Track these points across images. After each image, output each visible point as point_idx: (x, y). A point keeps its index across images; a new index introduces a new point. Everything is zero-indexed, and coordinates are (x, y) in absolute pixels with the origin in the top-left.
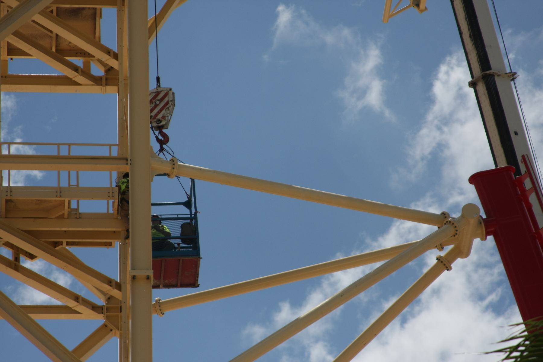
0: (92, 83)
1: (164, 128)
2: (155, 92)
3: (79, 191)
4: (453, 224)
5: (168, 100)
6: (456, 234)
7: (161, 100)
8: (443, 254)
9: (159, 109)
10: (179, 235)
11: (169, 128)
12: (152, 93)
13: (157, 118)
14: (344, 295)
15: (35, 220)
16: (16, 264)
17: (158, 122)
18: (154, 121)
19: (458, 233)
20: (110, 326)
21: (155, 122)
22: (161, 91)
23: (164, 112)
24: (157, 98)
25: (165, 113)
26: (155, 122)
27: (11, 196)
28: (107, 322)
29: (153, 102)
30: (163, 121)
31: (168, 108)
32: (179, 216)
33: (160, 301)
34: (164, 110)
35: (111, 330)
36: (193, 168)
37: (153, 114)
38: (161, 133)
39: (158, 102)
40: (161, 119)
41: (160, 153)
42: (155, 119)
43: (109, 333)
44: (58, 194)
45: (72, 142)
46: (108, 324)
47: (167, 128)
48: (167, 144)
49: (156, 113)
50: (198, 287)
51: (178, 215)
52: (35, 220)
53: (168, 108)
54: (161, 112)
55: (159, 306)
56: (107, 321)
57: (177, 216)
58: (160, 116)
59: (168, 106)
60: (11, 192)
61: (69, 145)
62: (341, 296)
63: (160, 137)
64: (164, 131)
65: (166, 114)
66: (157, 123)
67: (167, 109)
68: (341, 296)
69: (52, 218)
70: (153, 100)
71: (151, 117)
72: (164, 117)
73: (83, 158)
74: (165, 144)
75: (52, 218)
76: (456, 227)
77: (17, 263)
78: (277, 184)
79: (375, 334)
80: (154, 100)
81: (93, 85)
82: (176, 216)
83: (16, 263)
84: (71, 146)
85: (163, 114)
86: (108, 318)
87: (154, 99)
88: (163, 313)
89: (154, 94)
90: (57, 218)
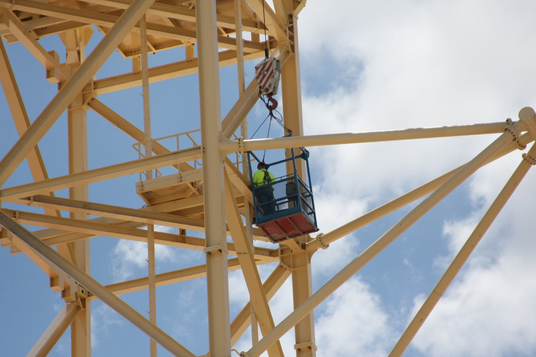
0: (260, 50)
2: (263, 64)
5: (273, 69)
6: (515, 138)
7: (267, 70)
8: (526, 151)
9: (266, 79)
11: (277, 93)
12: (261, 65)
13: (265, 87)
14: (403, 223)
16: (182, 237)
17: (266, 91)
18: (263, 90)
19: (516, 137)
20: (285, 266)
21: (264, 91)
22: (267, 62)
23: (270, 80)
24: (264, 69)
25: (270, 82)
26: (264, 91)
27: (143, 190)
28: (281, 263)
29: (262, 73)
30: (270, 89)
31: (273, 76)
33: (321, 236)
34: (270, 79)
35: (286, 269)
36: (259, 141)
37: (262, 84)
38: (270, 99)
39: (265, 73)
40: (268, 88)
42: (264, 89)
43: (285, 271)
44: (179, 180)
45: (136, 151)
46: (283, 264)
47: (276, 94)
48: (276, 109)
49: (264, 82)
50: (319, 231)
53: (273, 76)
54: (267, 81)
55: (320, 241)
56: (281, 262)
58: (267, 86)
59: (272, 75)
60: (143, 186)
62: (401, 224)
64: (273, 97)
65: (271, 82)
66: (266, 92)
67: (272, 78)
68: (401, 224)
69: (188, 198)
70: (262, 71)
71: (260, 87)
72: (270, 86)
75: (188, 198)
76: (512, 133)
77: (183, 236)
79: (480, 236)
80: (262, 72)
81: (259, 51)
84: (179, 136)
85: (270, 83)
86: (282, 260)
87: (262, 70)
88: (327, 246)
89: (262, 66)
90: (191, 196)
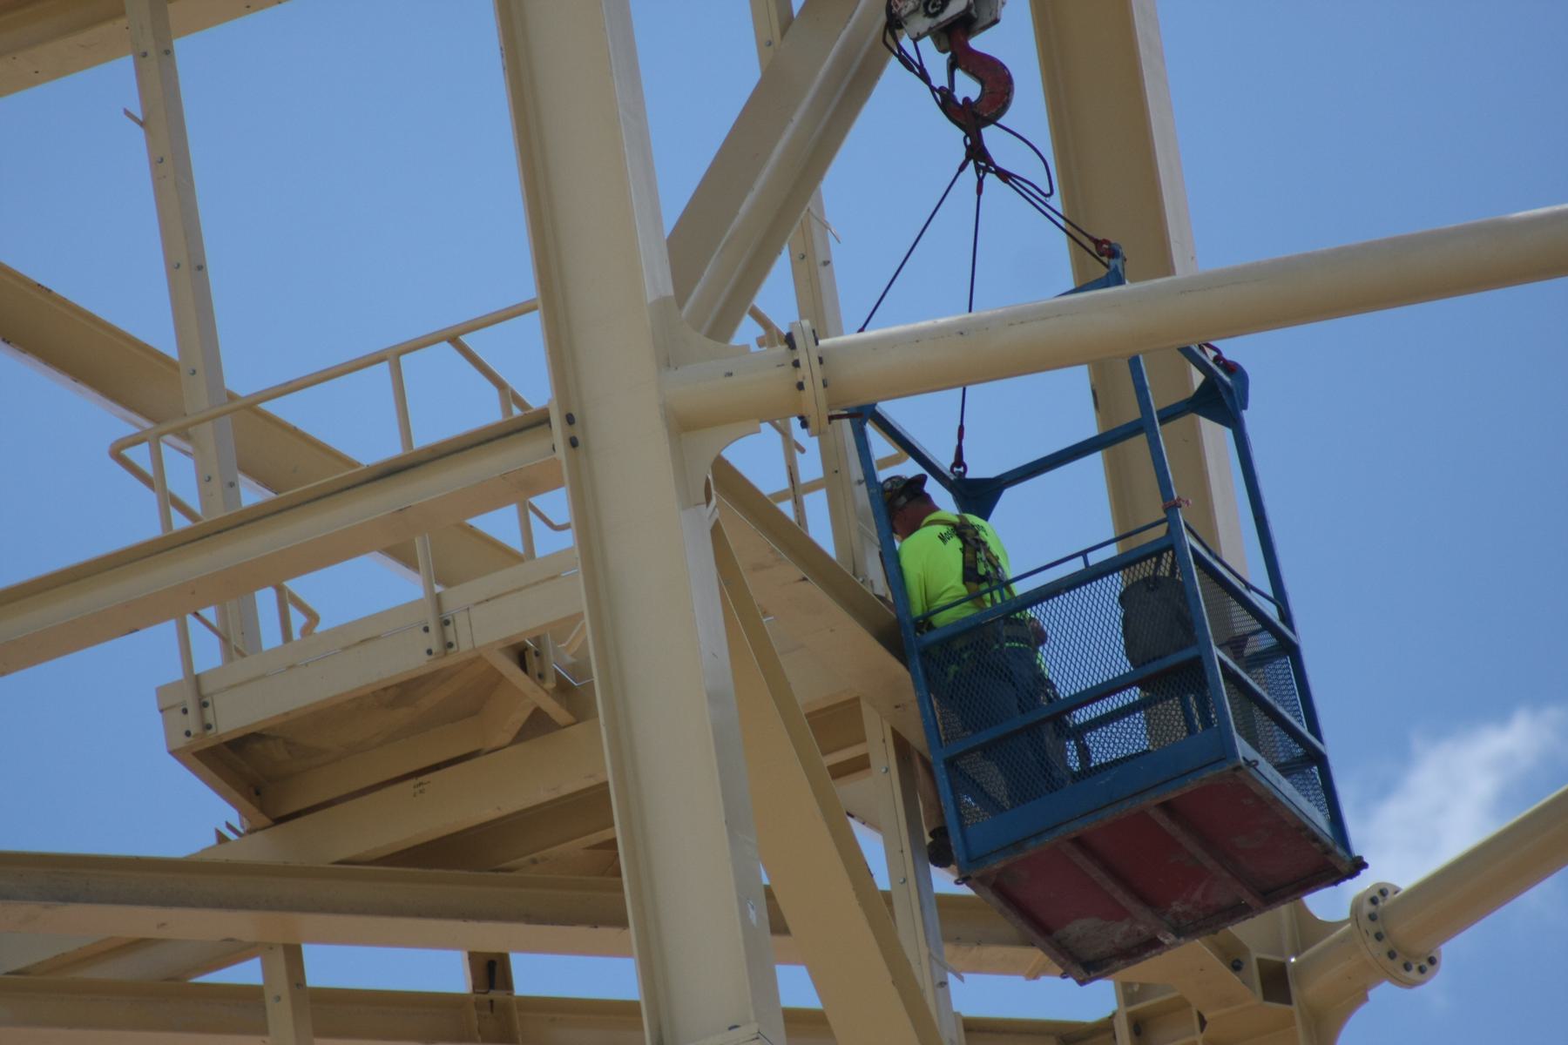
1: (980, 25)
3: (563, 575)
4: (1392, 955)
10: (1123, 666)
15: (421, 784)
21: (915, 11)
32: (1095, 558)
38: (963, 59)
41: (985, 181)
47: (996, 21)
50: (1363, 872)
51: (1084, 553)
52: (421, 784)
57: (1080, 559)
61: (392, 357)
63: (967, 88)
66: (928, 14)
73: (341, 491)
74: (992, 120)
78: (419, 914)
82: (1077, 565)
83: (488, 997)
